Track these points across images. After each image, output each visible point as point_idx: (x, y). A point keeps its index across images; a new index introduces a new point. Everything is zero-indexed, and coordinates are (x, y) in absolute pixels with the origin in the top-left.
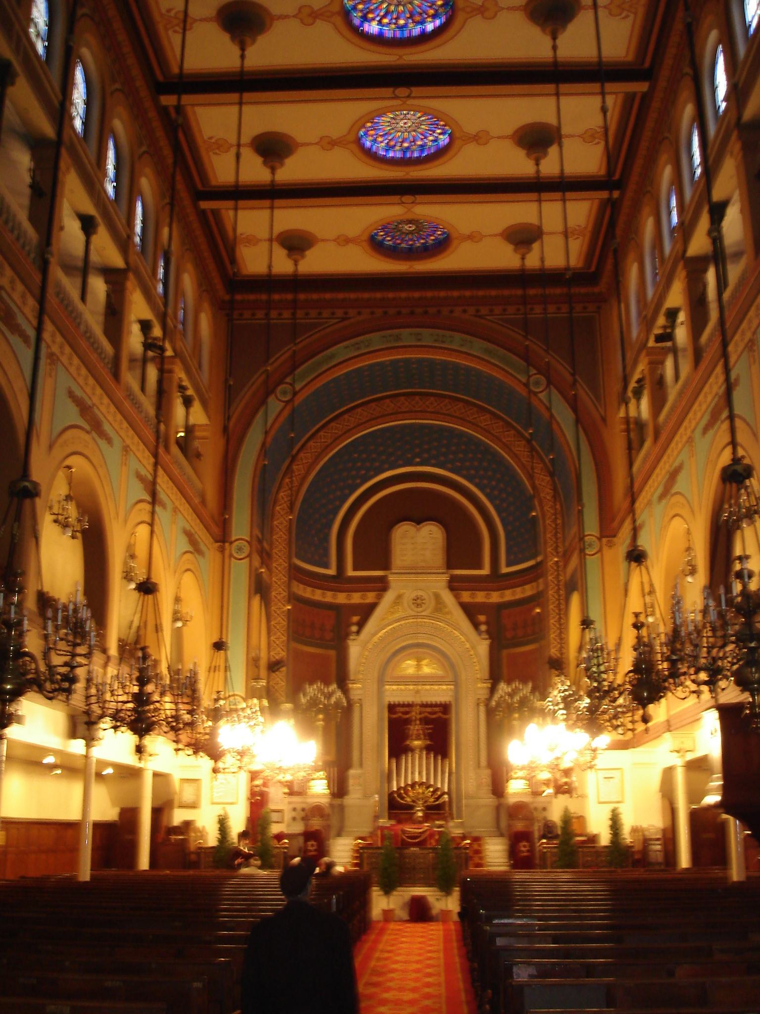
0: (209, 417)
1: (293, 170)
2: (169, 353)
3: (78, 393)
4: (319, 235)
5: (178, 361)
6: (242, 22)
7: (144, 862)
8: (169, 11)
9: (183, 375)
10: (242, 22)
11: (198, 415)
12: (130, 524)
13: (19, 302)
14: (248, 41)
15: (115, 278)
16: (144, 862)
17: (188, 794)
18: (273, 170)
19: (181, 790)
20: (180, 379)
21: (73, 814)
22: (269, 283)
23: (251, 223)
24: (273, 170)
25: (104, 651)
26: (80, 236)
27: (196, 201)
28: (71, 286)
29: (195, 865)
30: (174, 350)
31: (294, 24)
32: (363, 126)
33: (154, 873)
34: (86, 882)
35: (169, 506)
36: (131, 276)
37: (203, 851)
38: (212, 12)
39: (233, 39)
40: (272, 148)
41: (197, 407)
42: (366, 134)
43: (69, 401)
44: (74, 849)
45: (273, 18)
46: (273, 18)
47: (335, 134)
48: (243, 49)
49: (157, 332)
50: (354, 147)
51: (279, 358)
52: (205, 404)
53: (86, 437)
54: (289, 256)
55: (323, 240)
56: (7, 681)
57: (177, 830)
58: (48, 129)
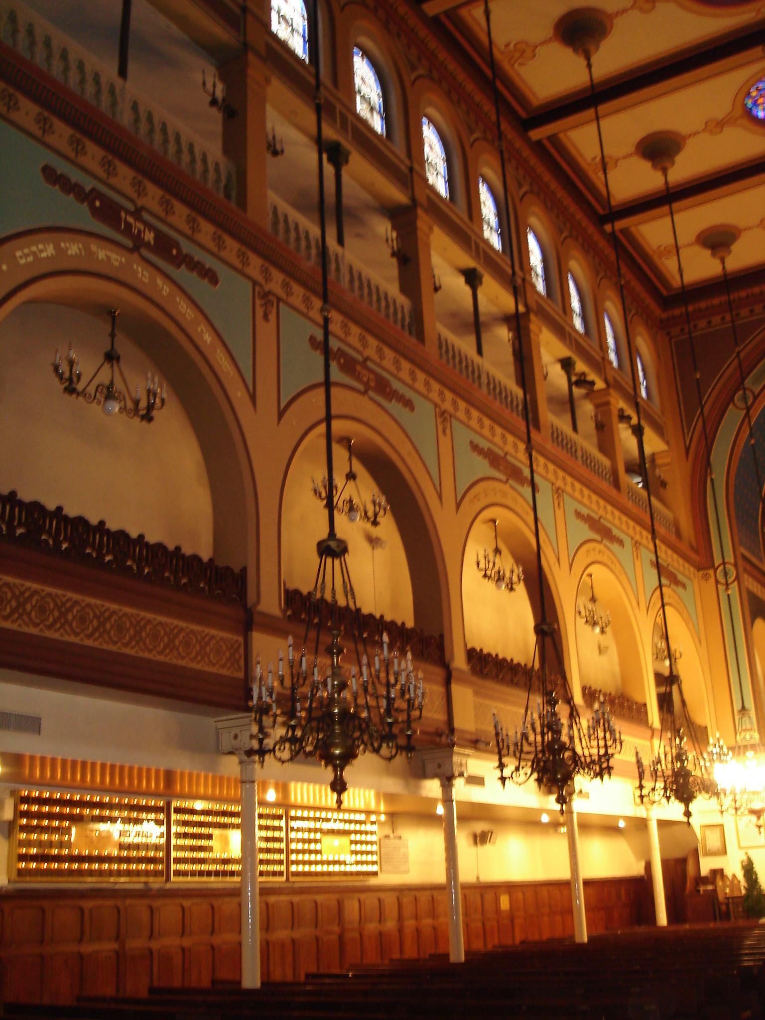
0: (667, 443)
1: (685, 167)
2: (600, 385)
3: (484, 445)
4: (741, 224)
5: (612, 391)
6: (580, 30)
7: (662, 918)
8: (507, 45)
9: (622, 404)
10: (580, 30)
11: (653, 443)
12: (578, 568)
13: (393, 369)
14: (592, 48)
15: (517, 323)
16: (662, 918)
17: (713, 840)
18: (665, 171)
19: (704, 838)
20: (621, 411)
21: (562, 873)
22: (15, 257)
23: (653, 232)
24: (665, 171)
25: (569, 700)
26: (467, 290)
27: (598, 226)
28: (466, 345)
29: (726, 916)
30: (606, 381)
31: (635, 14)
32: (748, 94)
33: (674, 928)
34: (583, 944)
35: (628, 542)
36: (532, 317)
37: (733, 900)
38: (549, 32)
39: (575, 50)
40: (658, 149)
41: (649, 435)
42: (755, 103)
43: (475, 455)
44: (568, 911)
45: (611, 17)
46: (611, 17)
47: (720, 114)
48: (588, 58)
49: (580, 366)
50: (745, 122)
51: (730, 364)
52: (660, 430)
53: (506, 488)
54: (714, 255)
55: (745, 230)
56: (336, 746)
57: (705, 880)
58: (398, 195)
